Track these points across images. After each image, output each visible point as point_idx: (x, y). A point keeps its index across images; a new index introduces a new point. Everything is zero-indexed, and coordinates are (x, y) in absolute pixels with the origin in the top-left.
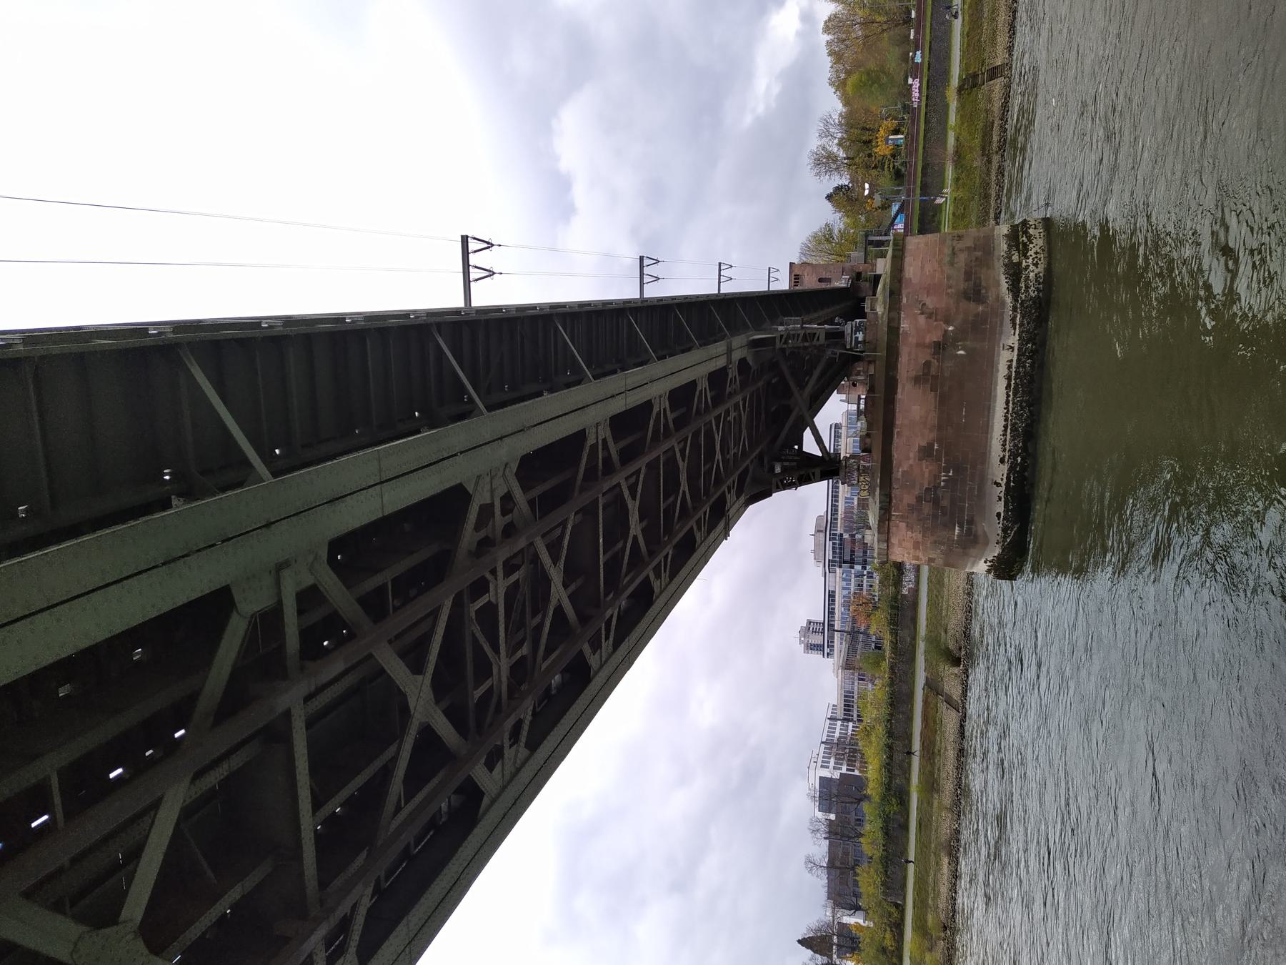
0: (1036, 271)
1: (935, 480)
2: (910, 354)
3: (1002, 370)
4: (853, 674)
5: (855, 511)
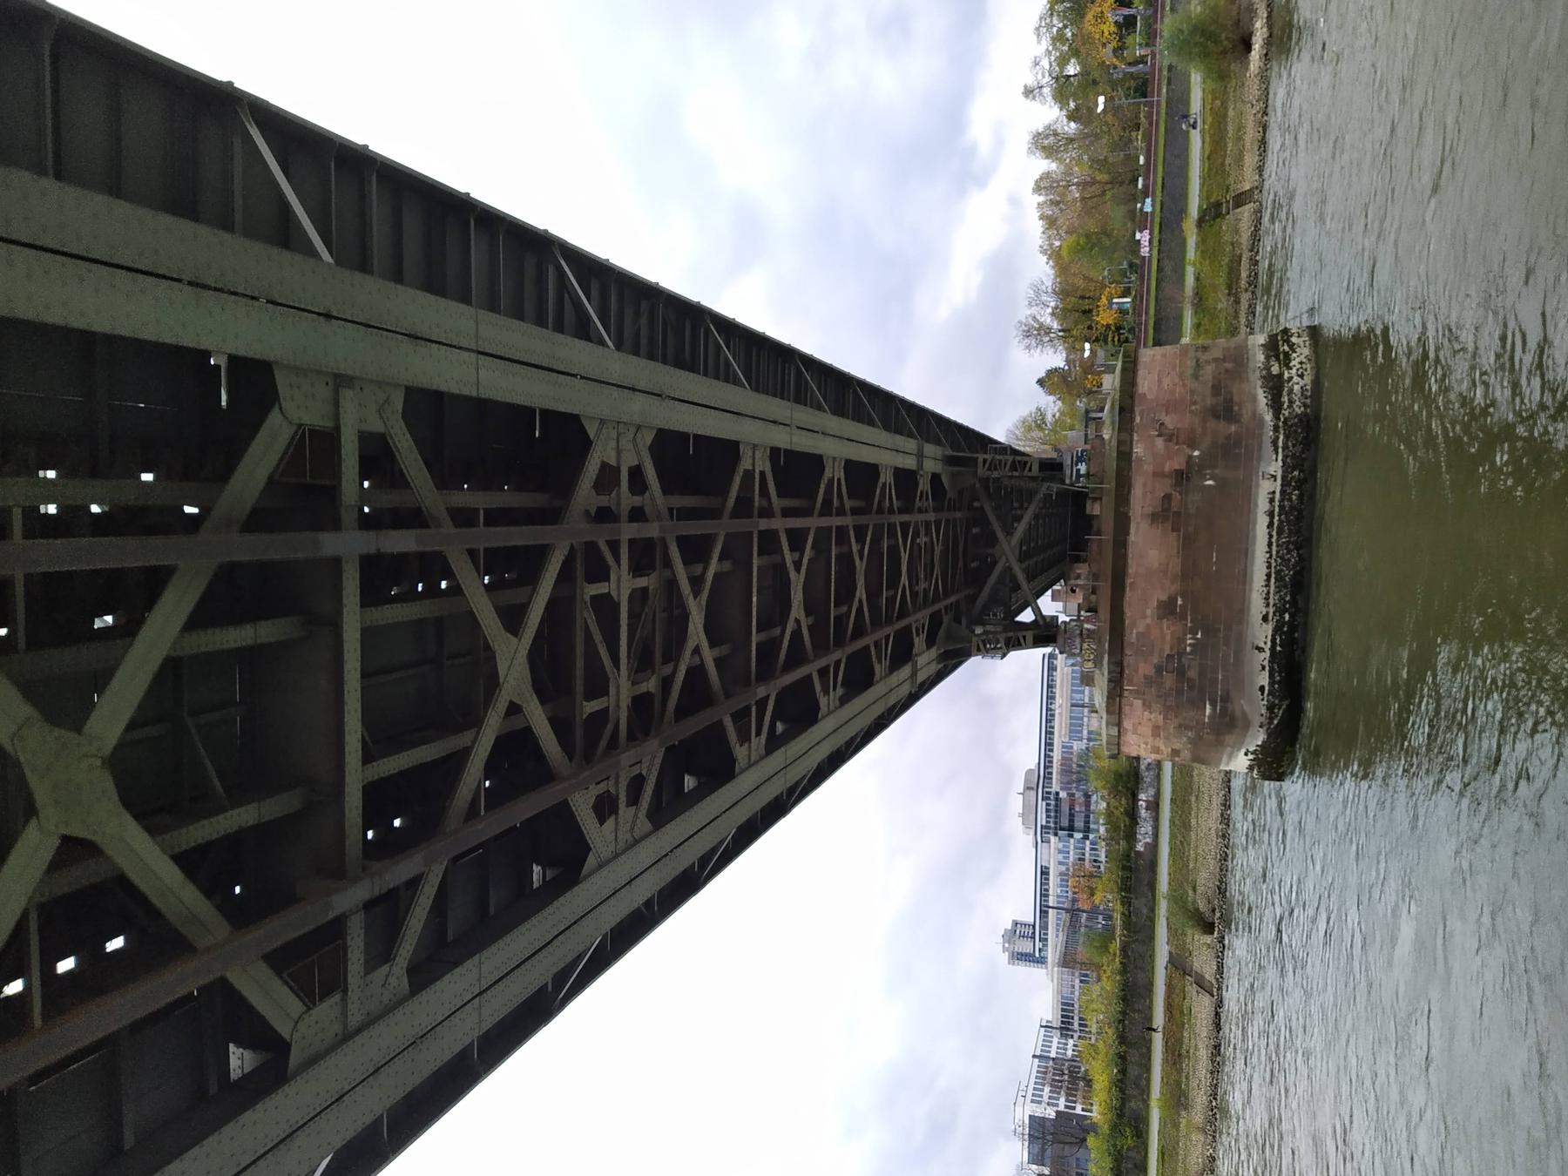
0: (1302, 383)
1: (1179, 644)
2: (1145, 485)
3: (1263, 505)
4: (1073, 974)
5: (1075, 760)
